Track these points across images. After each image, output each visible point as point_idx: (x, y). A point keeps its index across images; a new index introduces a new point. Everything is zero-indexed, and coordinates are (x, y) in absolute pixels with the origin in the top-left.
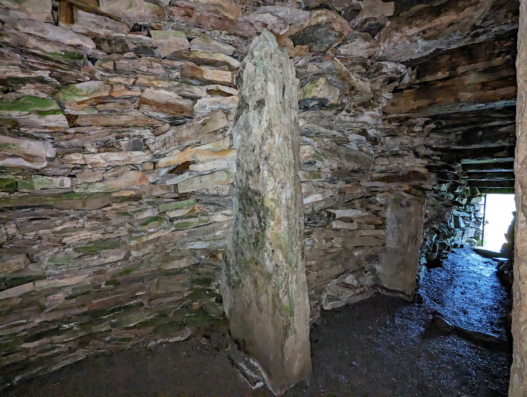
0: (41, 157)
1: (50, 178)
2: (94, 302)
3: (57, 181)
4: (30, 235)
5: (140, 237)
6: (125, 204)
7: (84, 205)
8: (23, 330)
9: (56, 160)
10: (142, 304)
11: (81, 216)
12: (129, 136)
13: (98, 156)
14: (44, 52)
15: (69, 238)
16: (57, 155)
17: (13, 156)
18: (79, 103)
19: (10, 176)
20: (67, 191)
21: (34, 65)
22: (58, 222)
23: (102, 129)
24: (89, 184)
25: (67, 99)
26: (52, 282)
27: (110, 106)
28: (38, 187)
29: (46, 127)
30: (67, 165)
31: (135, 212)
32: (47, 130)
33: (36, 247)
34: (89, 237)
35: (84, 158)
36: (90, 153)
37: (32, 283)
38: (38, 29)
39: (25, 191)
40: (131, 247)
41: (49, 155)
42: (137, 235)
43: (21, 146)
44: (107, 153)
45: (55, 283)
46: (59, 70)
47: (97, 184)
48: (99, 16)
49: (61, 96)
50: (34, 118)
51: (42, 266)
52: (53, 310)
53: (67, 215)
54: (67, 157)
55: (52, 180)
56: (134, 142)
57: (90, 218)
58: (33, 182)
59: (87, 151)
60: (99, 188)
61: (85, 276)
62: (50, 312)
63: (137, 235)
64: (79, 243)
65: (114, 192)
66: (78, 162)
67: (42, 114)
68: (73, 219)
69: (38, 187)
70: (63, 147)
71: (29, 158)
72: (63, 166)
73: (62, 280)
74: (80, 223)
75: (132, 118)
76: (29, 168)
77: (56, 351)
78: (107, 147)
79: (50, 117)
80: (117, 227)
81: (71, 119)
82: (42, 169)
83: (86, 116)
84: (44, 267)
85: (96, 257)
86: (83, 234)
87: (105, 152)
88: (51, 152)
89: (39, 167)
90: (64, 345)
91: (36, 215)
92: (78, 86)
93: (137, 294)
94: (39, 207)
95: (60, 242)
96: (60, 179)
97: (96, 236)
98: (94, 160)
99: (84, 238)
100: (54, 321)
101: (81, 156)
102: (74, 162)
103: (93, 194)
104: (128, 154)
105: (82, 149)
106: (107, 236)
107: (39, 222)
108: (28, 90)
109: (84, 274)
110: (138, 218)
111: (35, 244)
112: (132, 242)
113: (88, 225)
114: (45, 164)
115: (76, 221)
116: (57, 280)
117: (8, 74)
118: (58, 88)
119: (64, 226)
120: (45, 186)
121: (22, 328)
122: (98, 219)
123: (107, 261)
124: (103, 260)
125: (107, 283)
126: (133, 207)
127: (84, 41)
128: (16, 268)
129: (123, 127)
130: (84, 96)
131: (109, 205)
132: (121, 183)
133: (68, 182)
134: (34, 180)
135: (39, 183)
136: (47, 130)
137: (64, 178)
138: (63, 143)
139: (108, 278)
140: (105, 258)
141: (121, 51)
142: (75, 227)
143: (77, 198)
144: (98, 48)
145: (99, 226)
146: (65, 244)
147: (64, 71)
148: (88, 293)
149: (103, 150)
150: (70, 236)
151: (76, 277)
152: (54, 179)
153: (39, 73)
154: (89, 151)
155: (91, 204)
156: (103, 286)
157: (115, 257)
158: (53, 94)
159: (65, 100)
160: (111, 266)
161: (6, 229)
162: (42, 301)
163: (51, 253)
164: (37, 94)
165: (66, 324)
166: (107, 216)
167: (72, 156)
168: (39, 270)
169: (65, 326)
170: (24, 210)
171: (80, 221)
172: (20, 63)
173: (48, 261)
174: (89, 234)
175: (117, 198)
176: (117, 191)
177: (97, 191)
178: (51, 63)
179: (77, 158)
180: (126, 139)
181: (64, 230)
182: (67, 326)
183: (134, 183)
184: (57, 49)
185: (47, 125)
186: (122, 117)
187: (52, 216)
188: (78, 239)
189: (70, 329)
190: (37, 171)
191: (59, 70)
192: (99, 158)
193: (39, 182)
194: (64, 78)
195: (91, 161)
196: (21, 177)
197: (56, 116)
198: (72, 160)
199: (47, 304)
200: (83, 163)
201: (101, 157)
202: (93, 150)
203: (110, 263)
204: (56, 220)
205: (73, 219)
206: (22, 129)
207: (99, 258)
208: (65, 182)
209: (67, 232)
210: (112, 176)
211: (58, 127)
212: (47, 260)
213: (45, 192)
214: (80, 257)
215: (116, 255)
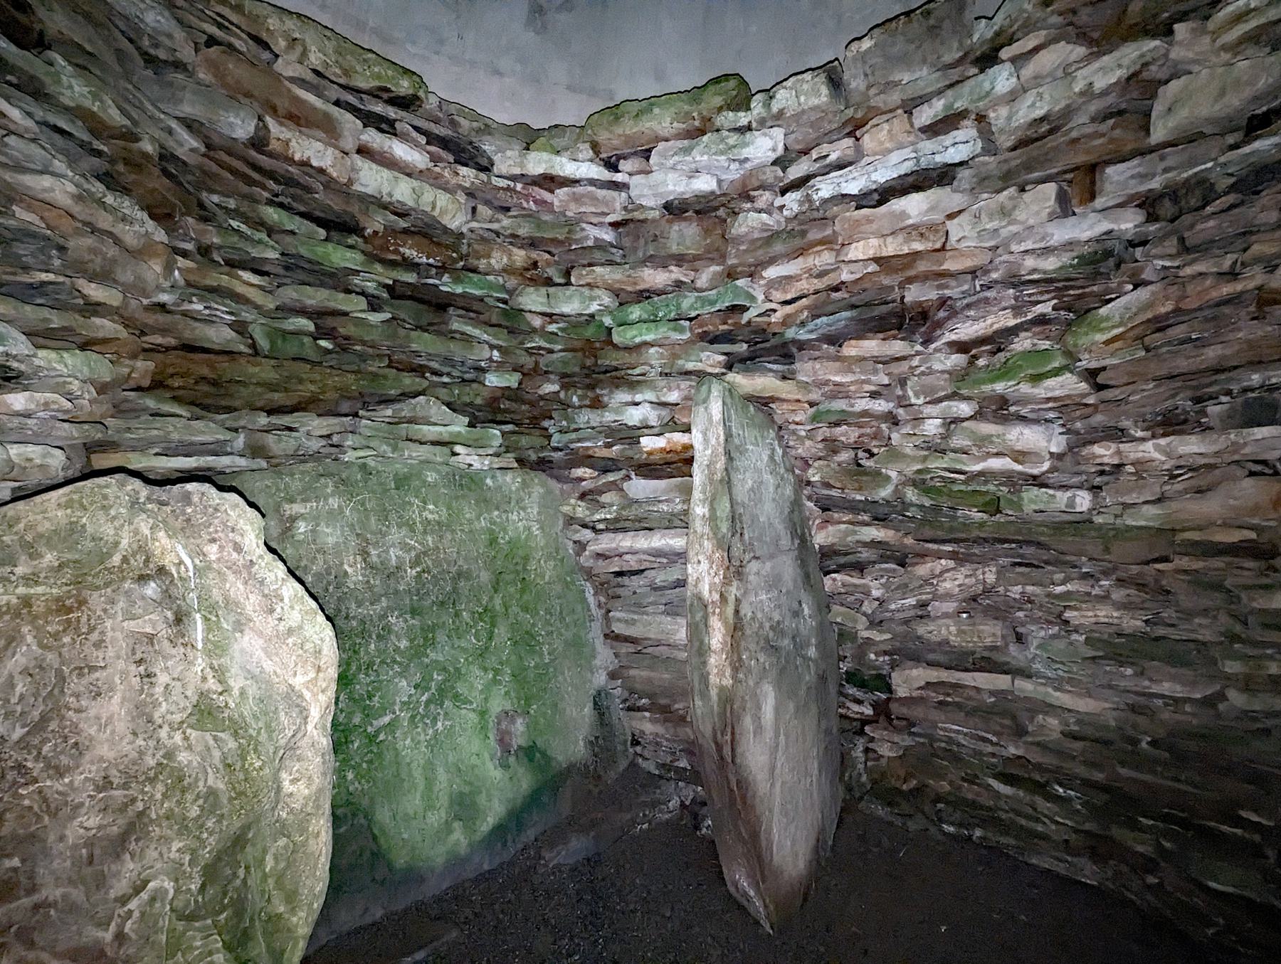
0: (1036, 454)
1: (1051, 492)
2: (1124, 771)
3: (1062, 497)
4: (1016, 591)
5: (1260, 657)
6: (1218, 563)
7: (1107, 550)
8: (993, 755)
9: (1068, 458)
10: (1257, 852)
11: (1106, 573)
12: (1229, 393)
13: (1149, 446)
14: (1045, 273)
15: (1076, 613)
16: (1070, 448)
17: (997, 454)
18: (1107, 342)
19: (991, 488)
20: (1078, 518)
21: (1032, 299)
22: (1059, 576)
23: (1155, 387)
24: (1126, 506)
25: (1080, 342)
26: (1041, 689)
27: (1178, 332)
28: (1029, 508)
29: (1049, 400)
30: (1083, 468)
31: (1247, 588)
32: (1050, 405)
33: (1021, 614)
34: (1116, 621)
35: (1119, 452)
36: (1134, 440)
37: (1009, 677)
38: (1038, 237)
39: (1010, 513)
40: (1228, 677)
41: (1054, 449)
42: (1250, 652)
43: (1008, 437)
44: (1172, 438)
45: (1047, 694)
46: (1072, 292)
47: (1146, 507)
48: (1148, 157)
49: (1070, 340)
50: (1025, 388)
51: (1027, 653)
52: (1038, 744)
53: (1075, 567)
54: (1085, 451)
55: (1053, 496)
56: (1247, 404)
57: (1121, 582)
58: (1022, 499)
59: (1130, 435)
60: (1148, 516)
61: (1107, 705)
62: (1032, 743)
63: (1250, 652)
64: (1095, 627)
65: (1183, 530)
66: (1106, 460)
67: (1037, 379)
68: (1087, 576)
69: (1029, 508)
70: (1077, 433)
71: (1020, 456)
72: (1077, 469)
73: (1058, 694)
74: (1101, 586)
75: (1237, 347)
76: (1020, 473)
77: (1040, 828)
78: (1170, 424)
79: (1050, 382)
80: (1189, 615)
81: (1091, 375)
82: (1043, 474)
83: (1114, 367)
84: (1030, 656)
85: (1129, 671)
86: (1104, 613)
87: (1164, 435)
88: (1057, 444)
89: (1035, 471)
90: (1054, 827)
91: (1021, 556)
92: (1103, 311)
93: (1244, 814)
94: (1029, 543)
95: (1060, 616)
96: (1069, 494)
97: (1133, 623)
98: (1140, 455)
99: (1106, 620)
100: (1038, 767)
101: (1113, 446)
102: (1098, 461)
103: (1130, 529)
104: (1232, 436)
105: (1117, 434)
106: (1161, 631)
107: (1028, 570)
108: (1023, 343)
109: (1106, 700)
110: (1255, 605)
111: (1020, 609)
112: (1228, 663)
113: (1119, 594)
114: (1046, 466)
115: (1092, 582)
116: (1050, 690)
117: (996, 327)
118: (1069, 324)
119: (1069, 587)
120: (1042, 507)
121: (990, 749)
122: (1141, 586)
123: (1155, 689)
124: (1147, 683)
125: (1153, 743)
126: (1246, 573)
127: (1115, 221)
128: (988, 641)
129: (1218, 371)
130: (1114, 327)
131: (1165, 559)
132: (1211, 507)
133: (1084, 501)
134: (1024, 495)
135: (1031, 501)
136: (1050, 405)
137: (1080, 493)
138: (1078, 425)
139: (1161, 733)
140: (1151, 680)
141: (1199, 204)
142: (1089, 594)
143: (1093, 533)
144: (1152, 218)
145: (1143, 602)
146: (1067, 622)
147: (1081, 291)
148: (1107, 743)
149: (796, 520)
150: (1076, 609)
151: (1088, 700)
152: (1059, 494)
153: (1040, 309)
154: (1133, 436)
155: (1120, 551)
156: (1144, 745)
157: (1178, 688)
158: (1060, 339)
159: (1075, 345)
160: (1166, 705)
161: (984, 573)
162: (1023, 717)
163: (1042, 633)
164: (1034, 345)
165: (1061, 786)
166: (1164, 583)
167: (1097, 449)
168: (1021, 657)
169: (1057, 787)
170: (1006, 546)
171: (1102, 583)
172: (1013, 302)
173: (1037, 647)
174: (1115, 614)
175: (1196, 544)
176: (1200, 528)
177: (1143, 523)
178: (1060, 285)
179: (1104, 452)
180: (1224, 399)
181: (1068, 595)
182: (1061, 790)
183: (1256, 510)
184: (1066, 259)
185: (1049, 395)
186: (1206, 350)
187: (1047, 563)
188: (1093, 620)
189: (1067, 800)
190: (1034, 477)
191: (1072, 292)
192: (1151, 450)
193: (1033, 499)
194: (1078, 305)
195: (1133, 456)
196: (1005, 489)
197: (1059, 379)
198: (1095, 456)
199: (1030, 729)
200: (1116, 462)
201: (1157, 448)
202: (1139, 434)
203: (1163, 696)
204: (1055, 573)
205: (1087, 576)
206: (1013, 409)
207: (1136, 674)
208: (1078, 500)
209: (1071, 600)
210: (1186, 491)
211: (1068, 396)
212: (1035, 644)
213: (1040, 517)
214: (1094, 658)
215: (1184, 685)
